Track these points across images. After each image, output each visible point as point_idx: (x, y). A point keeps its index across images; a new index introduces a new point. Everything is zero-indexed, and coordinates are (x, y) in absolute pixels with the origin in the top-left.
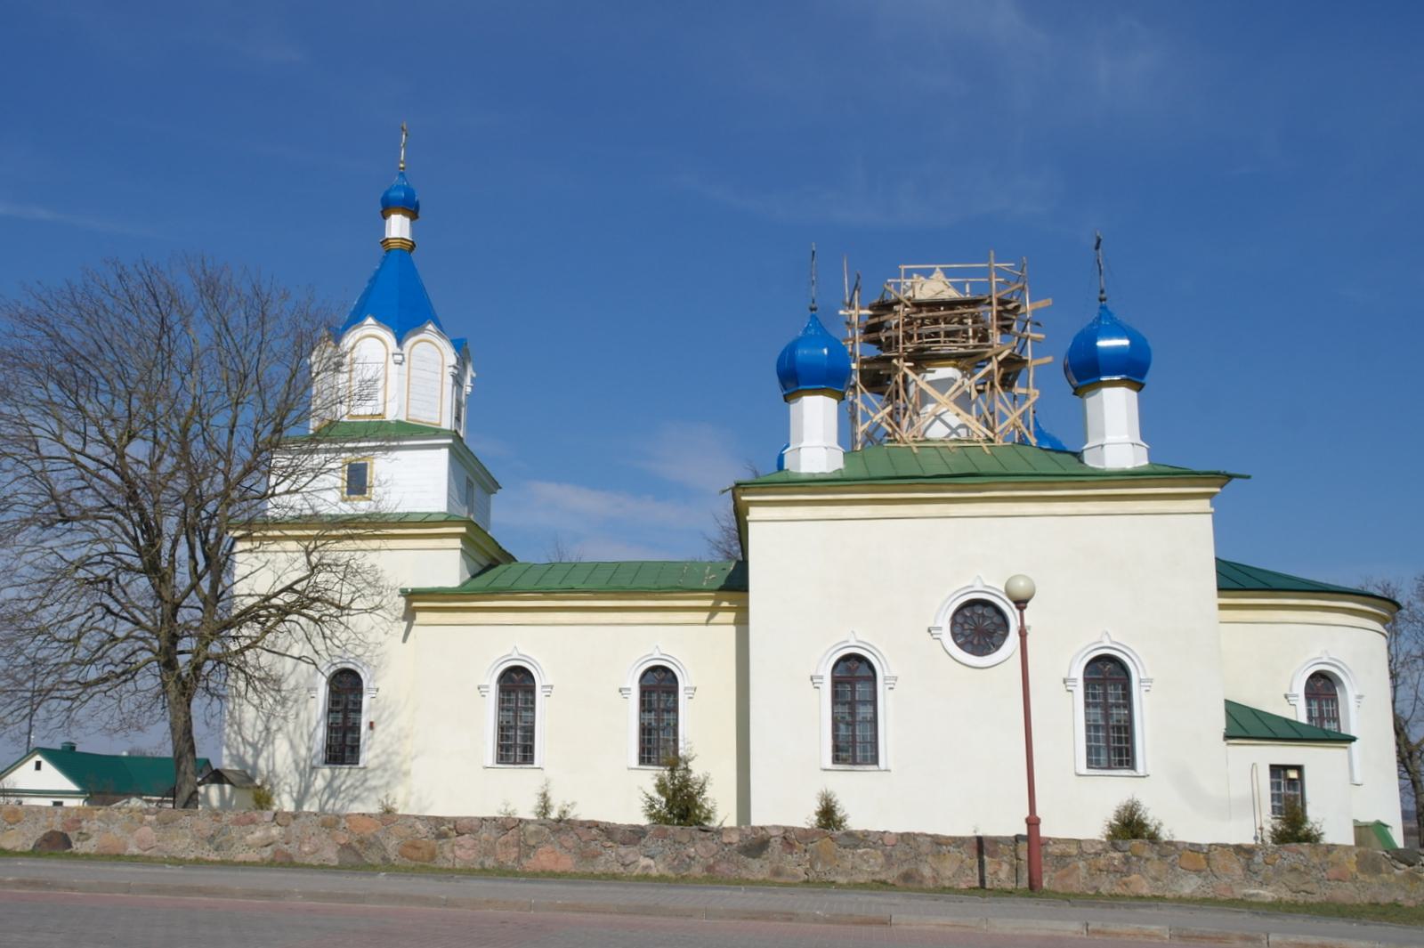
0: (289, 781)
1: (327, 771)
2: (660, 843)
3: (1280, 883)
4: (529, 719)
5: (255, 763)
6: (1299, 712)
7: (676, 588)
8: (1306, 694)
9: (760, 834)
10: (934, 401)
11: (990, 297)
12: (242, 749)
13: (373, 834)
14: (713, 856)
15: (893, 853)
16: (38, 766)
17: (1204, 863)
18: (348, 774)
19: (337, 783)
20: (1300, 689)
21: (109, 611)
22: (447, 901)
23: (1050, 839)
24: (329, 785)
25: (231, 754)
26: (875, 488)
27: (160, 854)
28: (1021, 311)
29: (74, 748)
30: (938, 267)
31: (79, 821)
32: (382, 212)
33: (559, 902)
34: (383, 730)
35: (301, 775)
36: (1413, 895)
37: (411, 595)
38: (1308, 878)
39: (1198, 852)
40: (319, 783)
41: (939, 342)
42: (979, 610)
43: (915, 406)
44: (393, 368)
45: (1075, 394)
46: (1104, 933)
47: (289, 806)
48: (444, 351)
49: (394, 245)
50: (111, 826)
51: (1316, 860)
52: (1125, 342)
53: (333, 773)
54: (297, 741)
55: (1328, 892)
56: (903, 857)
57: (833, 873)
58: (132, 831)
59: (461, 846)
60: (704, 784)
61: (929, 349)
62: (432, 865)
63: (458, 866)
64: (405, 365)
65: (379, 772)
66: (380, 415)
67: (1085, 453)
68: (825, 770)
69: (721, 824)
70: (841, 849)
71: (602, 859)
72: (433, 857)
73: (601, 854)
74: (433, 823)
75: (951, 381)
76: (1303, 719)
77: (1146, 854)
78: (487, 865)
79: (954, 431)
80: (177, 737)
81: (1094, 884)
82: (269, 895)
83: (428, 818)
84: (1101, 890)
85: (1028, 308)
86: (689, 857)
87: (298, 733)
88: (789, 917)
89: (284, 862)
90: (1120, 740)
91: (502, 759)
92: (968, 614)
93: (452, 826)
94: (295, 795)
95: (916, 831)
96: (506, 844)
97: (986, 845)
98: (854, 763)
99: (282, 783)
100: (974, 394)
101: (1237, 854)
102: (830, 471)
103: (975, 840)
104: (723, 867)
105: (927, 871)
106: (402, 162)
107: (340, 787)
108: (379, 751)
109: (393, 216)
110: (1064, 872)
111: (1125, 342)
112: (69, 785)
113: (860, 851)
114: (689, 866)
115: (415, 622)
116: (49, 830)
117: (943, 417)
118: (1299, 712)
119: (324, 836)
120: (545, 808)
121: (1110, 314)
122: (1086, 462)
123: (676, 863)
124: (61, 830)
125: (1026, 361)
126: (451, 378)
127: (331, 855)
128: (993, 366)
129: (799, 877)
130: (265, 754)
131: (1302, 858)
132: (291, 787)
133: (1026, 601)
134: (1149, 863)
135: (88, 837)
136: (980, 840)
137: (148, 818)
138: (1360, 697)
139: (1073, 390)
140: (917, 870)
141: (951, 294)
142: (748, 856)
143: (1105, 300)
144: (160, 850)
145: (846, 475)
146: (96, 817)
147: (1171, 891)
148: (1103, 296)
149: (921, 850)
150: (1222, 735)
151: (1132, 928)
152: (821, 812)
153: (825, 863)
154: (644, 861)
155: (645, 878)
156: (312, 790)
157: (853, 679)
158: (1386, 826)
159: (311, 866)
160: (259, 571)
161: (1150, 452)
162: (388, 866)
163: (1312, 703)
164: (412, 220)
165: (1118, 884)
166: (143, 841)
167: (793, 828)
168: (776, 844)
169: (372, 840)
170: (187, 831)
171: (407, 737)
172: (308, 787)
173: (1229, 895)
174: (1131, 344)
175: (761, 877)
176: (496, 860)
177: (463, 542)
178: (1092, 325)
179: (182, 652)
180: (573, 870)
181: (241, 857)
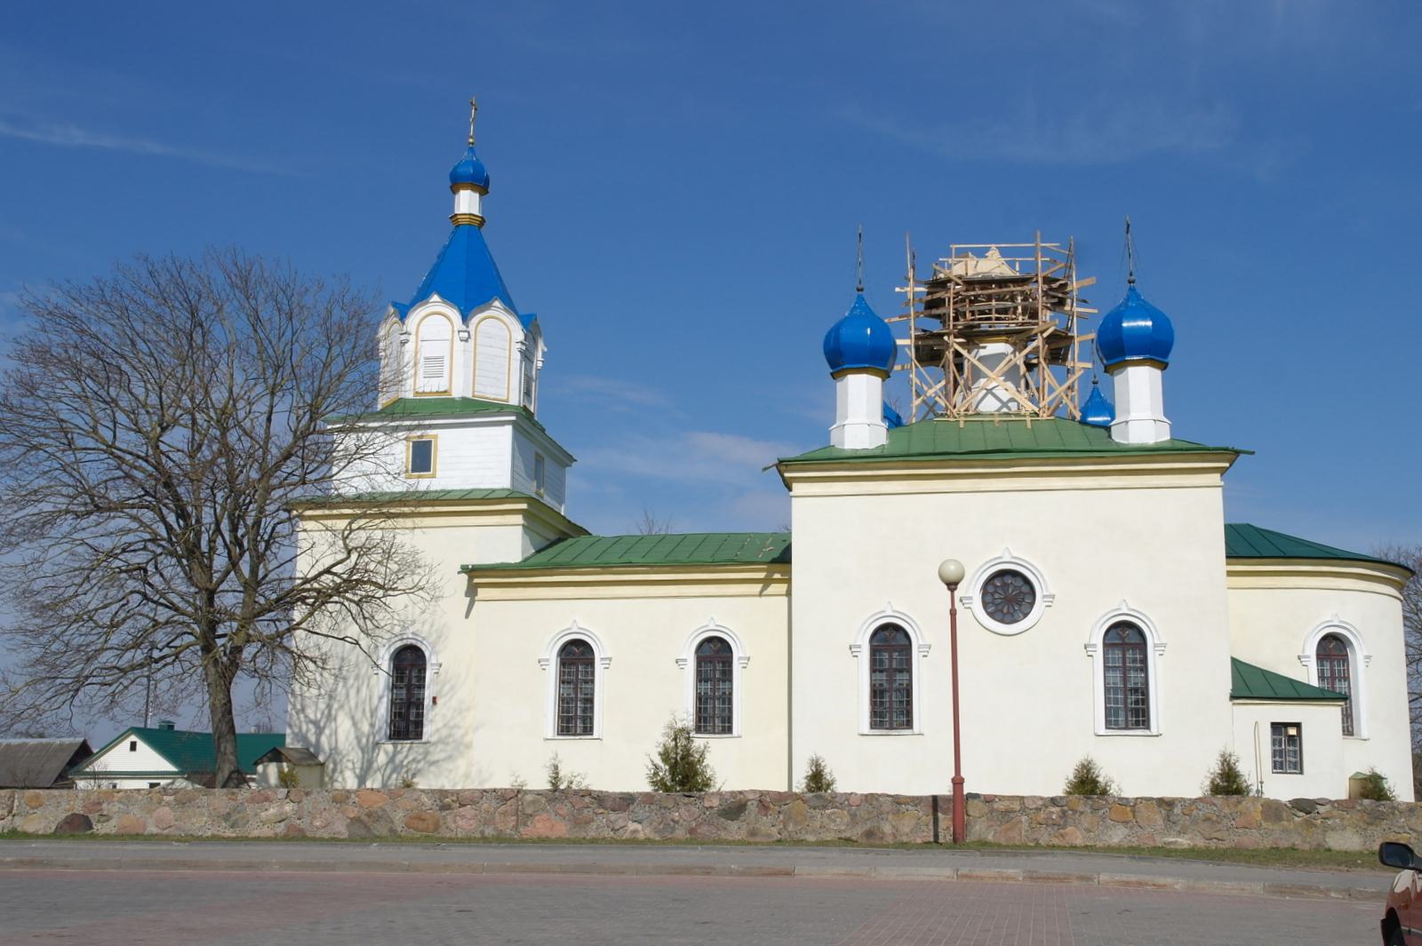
0: (351, 758)
1: (390, 747)
2: (647, 809)
3: (1196, 832)
4: (589, 691)
5: (318, 741)
6: (1309, 675)
7: (732, 560)
8: (1318, 655)
9: (738, 798)
10: (986, 376)
11: (1037, 275)
12: (304, 728)
13: (380, 807)
14: (695, 820)
15: (858, 813)
16: (133, 747)
17: (1131, 815)
18: (410, 749)
19: (399, 757)
20: (1312, 651)
21: (145, 596)
22: (409, 866)
23: (996, 796)
24: (392, 760)
25: (293, 733)
26: (910, 464)
27: (178, 833)
28: (1069, 289)
29: (171, 727)
30: (993, 246)
31: (100, 804)
32: (451, 187)
33: (508, 864)
34: (445, 704)
35: (363, 752)
36: (1308, 840)
37: (472, 571)
38: (1219, 826)
39: (1125, 805)
40: (382, 758)
41: (990, 319)
42: (1009, 580)
43: (966, 381)
44: (459, 345)
45: (1106, 371)
46: (970, 877)
47: (351, 783)
48: (511, 327)
49: (463, 221)
50: (130, 808)
51: (1227, 811)
52: (1149, 323)
53: (395, 747)
54: (358, 715)
55: (1236, 839)
56: (866, 817)
57: (804, 832)
58: (150, 812)
59: (463, 817)
60: (704, 751)
61: (979, 326)
62: (435, 835)
63: (460, 835)
64: (471, 341)
65: (440, 747)
66: (446, 392)
67: (1113, 428)
68: (863, 735)
69: (720, 789)
70: (811, 810)
71: (594, 825)
72: (437, 827)
73: (593, 821)
74: (437, 796)
75: (1001, 356)
76: (1315, 682)
77: (1081, 808)
78: (486, 834)
79: (1004, 404)
80: (216, 719)
81: (1035, 836)
82: (249, 866)
83: (433, 791)
84: (1041, 841)
85: (1074, 285)
86: (673, 821)
87: (360, 709)
88: (708, 871)
89: (296, 836)
90: (1137, 702)
91: (876, 725)
92: (999, 584)
93: (455, 798)
94: (358, 771)
95: (879, 792)
96: (504, 814)
97: (940, 803)
98: (891, 728)
99: (344, 760)
100: (1023, 369)
101: (1159, 806)
102: (873, 447)
103: (931, 799)
104: (704, 829)
105: (887, 829)
106: (471, 137)
107: (402, 761)
108: (440, 725)
109: (462, 192)
110: (1008, 825)
111: (1149, 323)
112: (167, 766)
113: (828, 812)
114: (673, 829)
115: (476, 598)
116: (70, 813)
117: (994, 391)
118: (1309, 675)
119: (334, 811)
120: (555, 779)
121: (1138, 296)
122: (1113, 438)
123: (662, 826)
124: (82, 813)
125: (1072, 337)
126: (519, 354)
127: (341, 828)
128: (1039, 342)
129: (773, 836)
130: (327, 731)
131: (1215, 808)
132: (353, 763)
133: (956, 584)
134: (1083, 816)
135: (108, 818)
136: (935, 798)
137: (167, 798)
138: (1368, 657)
139: (1103, 369)
140: (878, 828)
141: (1007, 272)
142: (728, 819)
143: (1133, 282)
144: (178, 829)
145: (886, 452)
146: (115, 799)
147: (1101, 840)
148: (1132, 278)
149: (882, 809)
150: (1228, 696)
151: (994, 871)
152: (811, 776)
153: (796, 823)
154: (632, 826)
155: (633, 842)
156: (375, 765)
157: (891, 647)
158: (1382, 778)
159: (321, 840)
160: (315, 549)
161: (1172, 428)
162: (395, 838)
163: (1325, 663)
164: (481, 195)
165: (1055, 836)
166: (162, 820)
167: (768, 792)
168: (752, 807)
169: (380, 813)
170: (204, 810)
171: (468, 709)
172: (370, 762)
173: (1151, 844)
174: (1153, 325)
175: (738, 837)
176: (495, 829)
177: (525, 518)
178: (1121, 305)
179: (220, 636)
180: (567, 836)
181: (255, 833)
